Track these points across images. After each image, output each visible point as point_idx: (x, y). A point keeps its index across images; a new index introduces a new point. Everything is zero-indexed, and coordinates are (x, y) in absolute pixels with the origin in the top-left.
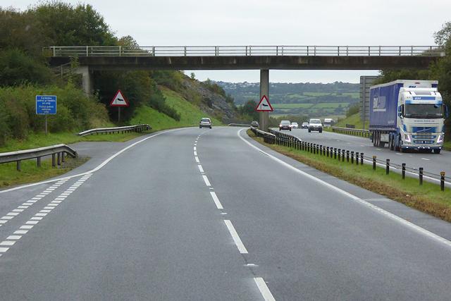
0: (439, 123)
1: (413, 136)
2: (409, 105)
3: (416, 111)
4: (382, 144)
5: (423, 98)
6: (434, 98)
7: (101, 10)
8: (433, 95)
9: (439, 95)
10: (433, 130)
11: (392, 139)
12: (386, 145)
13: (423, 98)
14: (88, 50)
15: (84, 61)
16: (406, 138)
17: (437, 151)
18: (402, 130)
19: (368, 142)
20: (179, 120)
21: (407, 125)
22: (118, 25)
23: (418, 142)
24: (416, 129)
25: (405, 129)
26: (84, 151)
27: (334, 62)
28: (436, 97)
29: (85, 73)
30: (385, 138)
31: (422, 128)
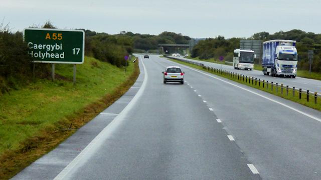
0: (295, 63)
1: (282, 69)
2: (280, 54)
3: (283, 57)
4: (268, 73)
5: (288, 51)
6: (293, 51)
7: (222, 35)
8: (292, 49)
9: (295, 49)
10: (291, 66)
11: (272, 71)
12: (270, 74)
13: (288, 51)
14: (163, 45)
15: (163, 46)
16: (279, 70)
17: (294, 77)
18: (277, 67)
19: (262, 73)
20: (148, 58)
21: (279, 64)
22: (109, 34)
23: (284, 72)
24: (284, 66)
25: (278, 66)
26: (143, 66)
27: (57, 35)
28: (294, 50)
29: (163, 48)
30: (269, 70)
31: (286, 65)
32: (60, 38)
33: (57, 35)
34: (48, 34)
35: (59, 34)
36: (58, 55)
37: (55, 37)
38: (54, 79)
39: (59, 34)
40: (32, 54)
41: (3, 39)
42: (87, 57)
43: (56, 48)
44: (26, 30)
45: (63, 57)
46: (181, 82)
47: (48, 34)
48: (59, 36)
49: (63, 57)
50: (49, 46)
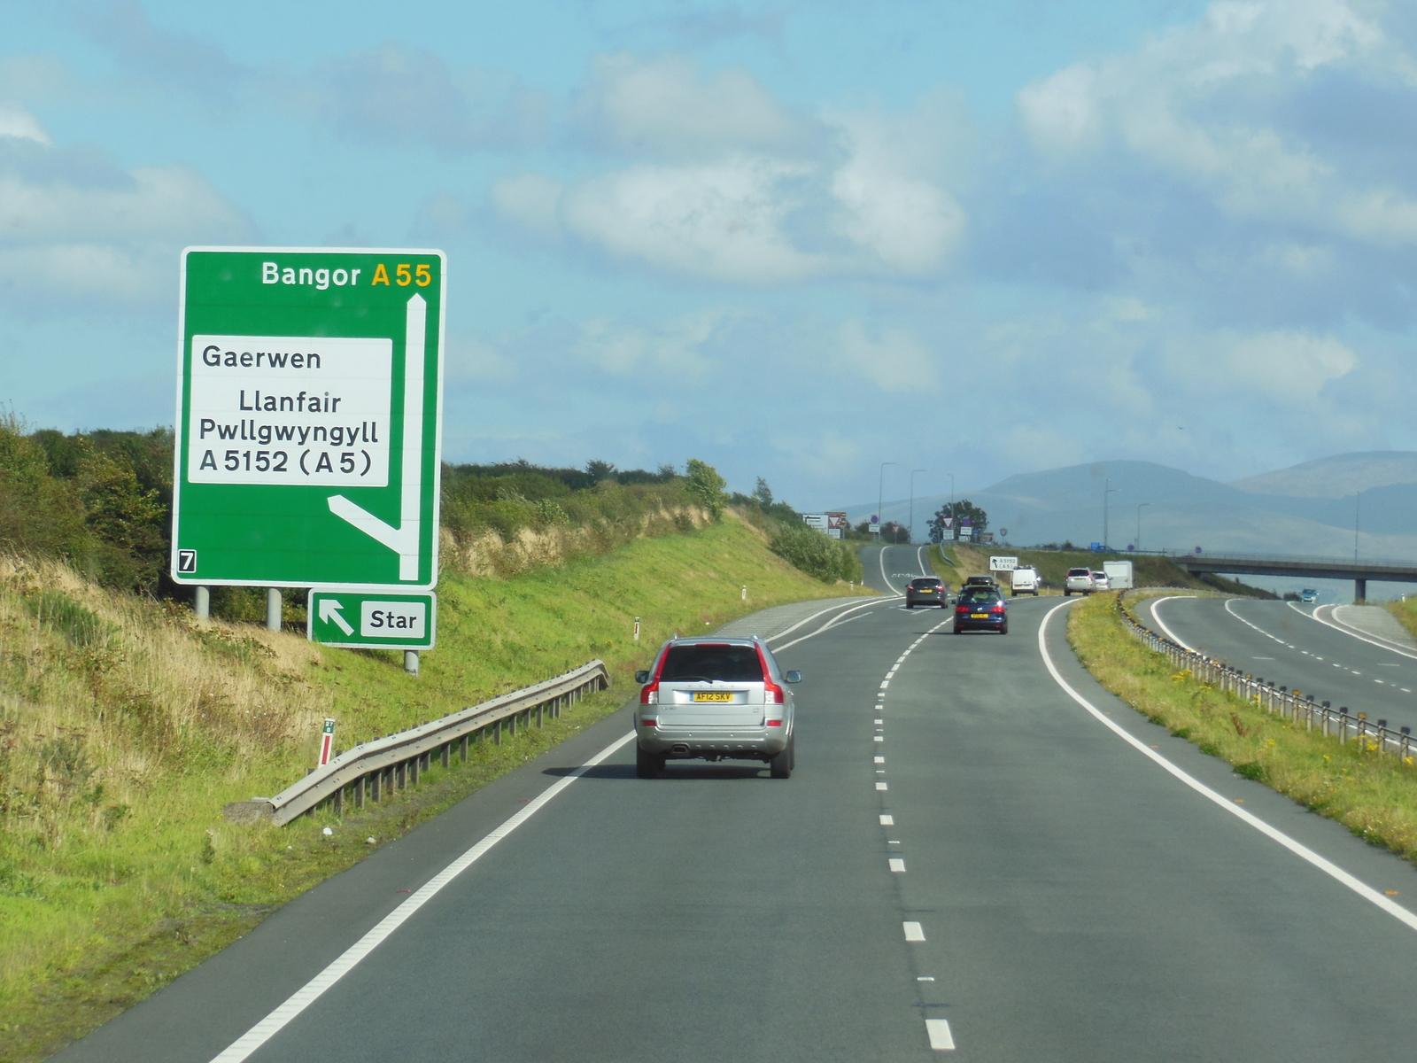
27: (412, 271)
32: (423, 278)
33: (412, 271)
34: (381, 267)
35: (419, 267)
36: (292, 275)
37: (403, 278)
38: (176, 960)
39: (419, 267)
40: (883, 695)
41: (522, 493)
42: (303, 620)
43: (326, 272)
44: (787, 778)
45: (266, 265)
46: (335, 401)
47: (381, 267)
48: (419, 273)
49: (266, 265)
50: (326, 272)
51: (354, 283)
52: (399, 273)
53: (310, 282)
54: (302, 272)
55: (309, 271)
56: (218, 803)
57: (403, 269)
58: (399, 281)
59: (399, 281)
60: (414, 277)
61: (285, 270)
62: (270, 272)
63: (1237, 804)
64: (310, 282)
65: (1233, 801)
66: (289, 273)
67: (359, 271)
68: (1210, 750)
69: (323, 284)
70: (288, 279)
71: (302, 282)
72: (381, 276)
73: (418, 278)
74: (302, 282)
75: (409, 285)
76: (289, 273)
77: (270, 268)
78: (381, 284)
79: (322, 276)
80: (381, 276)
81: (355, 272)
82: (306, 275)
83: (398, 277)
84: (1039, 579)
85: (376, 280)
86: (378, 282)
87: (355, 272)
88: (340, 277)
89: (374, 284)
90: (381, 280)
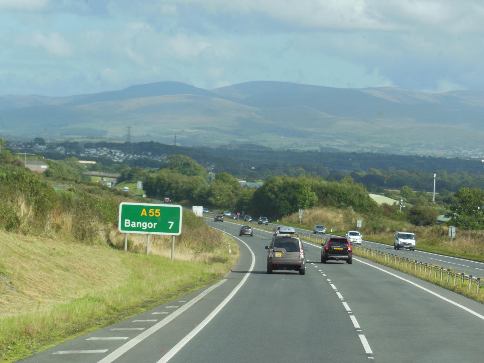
27: (154, 211)
34: (144, 210)
35: (156, 210)
37: (151, 214)
39: (156, 210)
47: (144, 210)
48: (156, 212)
50: (146, 223)
51: (154, 227)
52: (150, 212)
53: (140, 227)
54: (138, 223)
55: (140, 223)
56: (34, 310)
57: (151, 211)
58: (150, 215)
59: (150, 215)
60: (155, 214)
61: (132, 222)
62: (127, 223)
63: (460, 304)
64: (140, 227)
65: (437, 294)
66: (133, 223)
67: (156, 224)
68: (482, 302)
69: (144, 228)
70: (133, 225)
71: (138, 226)
72: (144, 213)
73: (156, 214)
74: (138, 226)
75: (152, 217)
76: (133, 223)
77: (127, 222)
78: (144, 216)
79: (144, 225)
80: (144, 213)
81: (155, 224)
82: (139, 225)
83: (149, 213)
84: (242, 186)
85: (142, 214)
86: (143, 215)
87: (155, 224)
88: (150, 225)
89: (142, 215)
90: (144, 214)
